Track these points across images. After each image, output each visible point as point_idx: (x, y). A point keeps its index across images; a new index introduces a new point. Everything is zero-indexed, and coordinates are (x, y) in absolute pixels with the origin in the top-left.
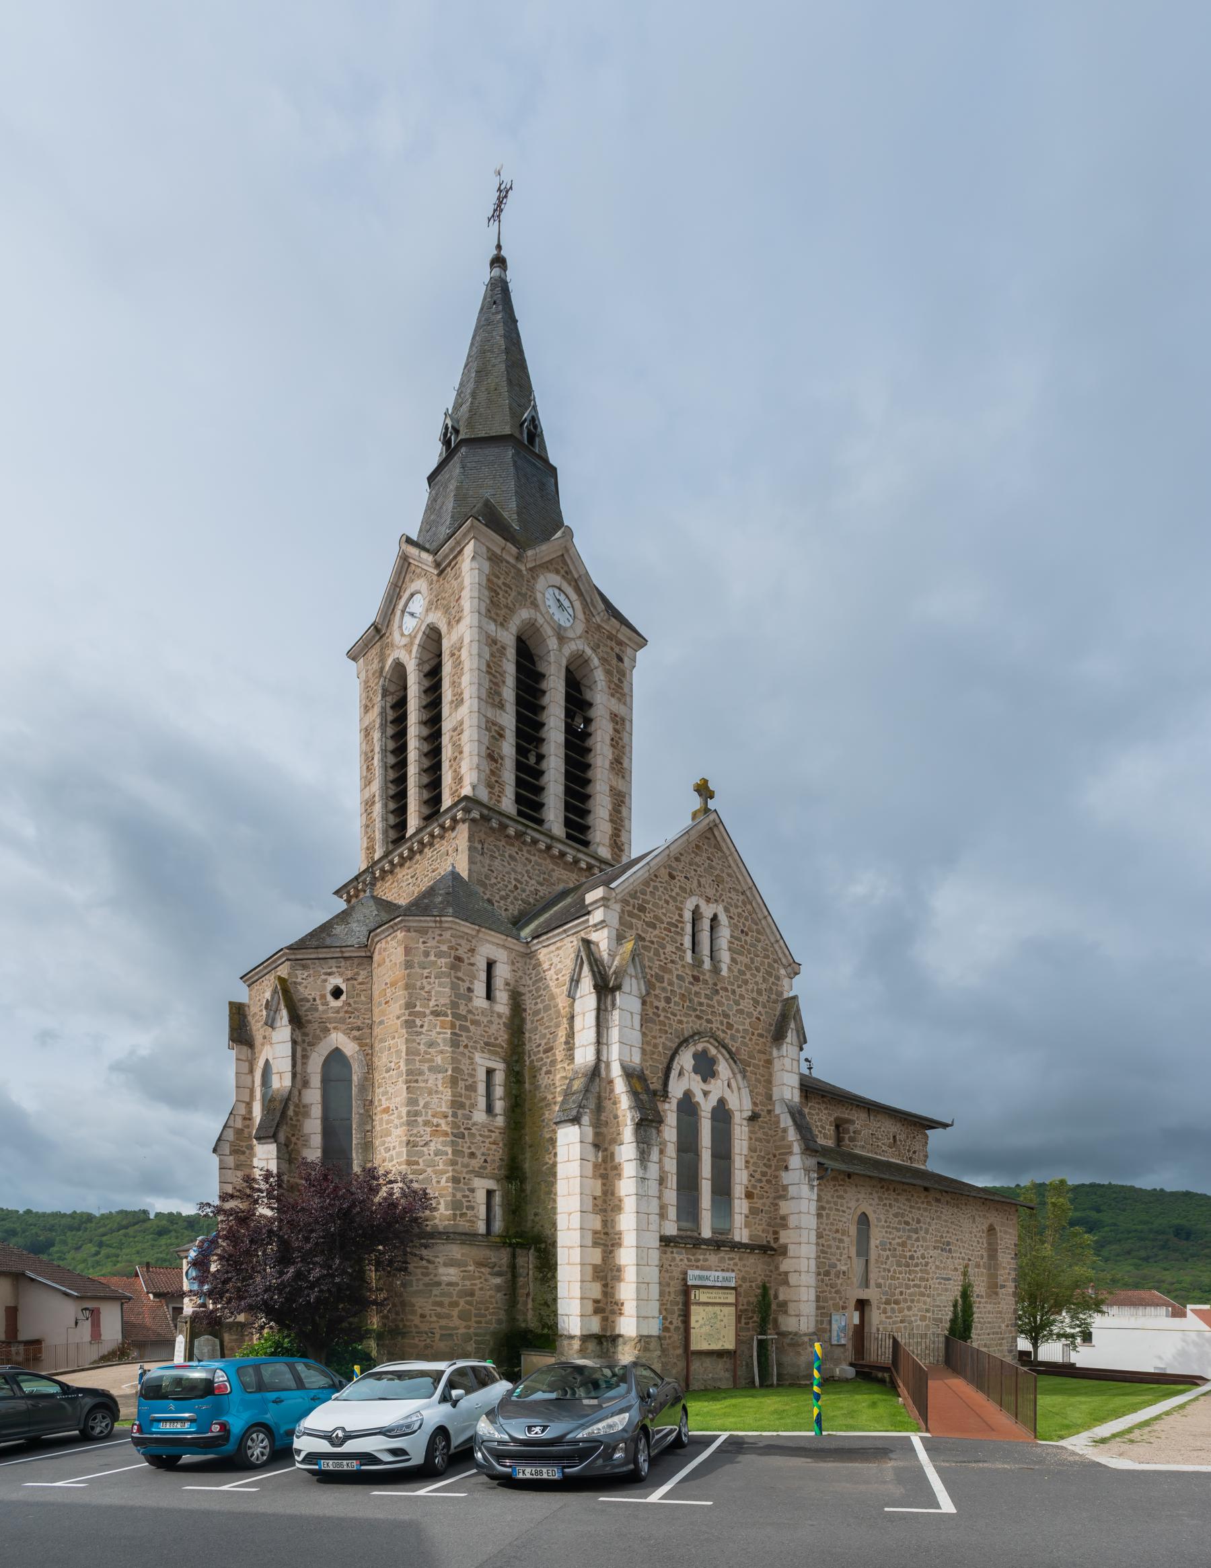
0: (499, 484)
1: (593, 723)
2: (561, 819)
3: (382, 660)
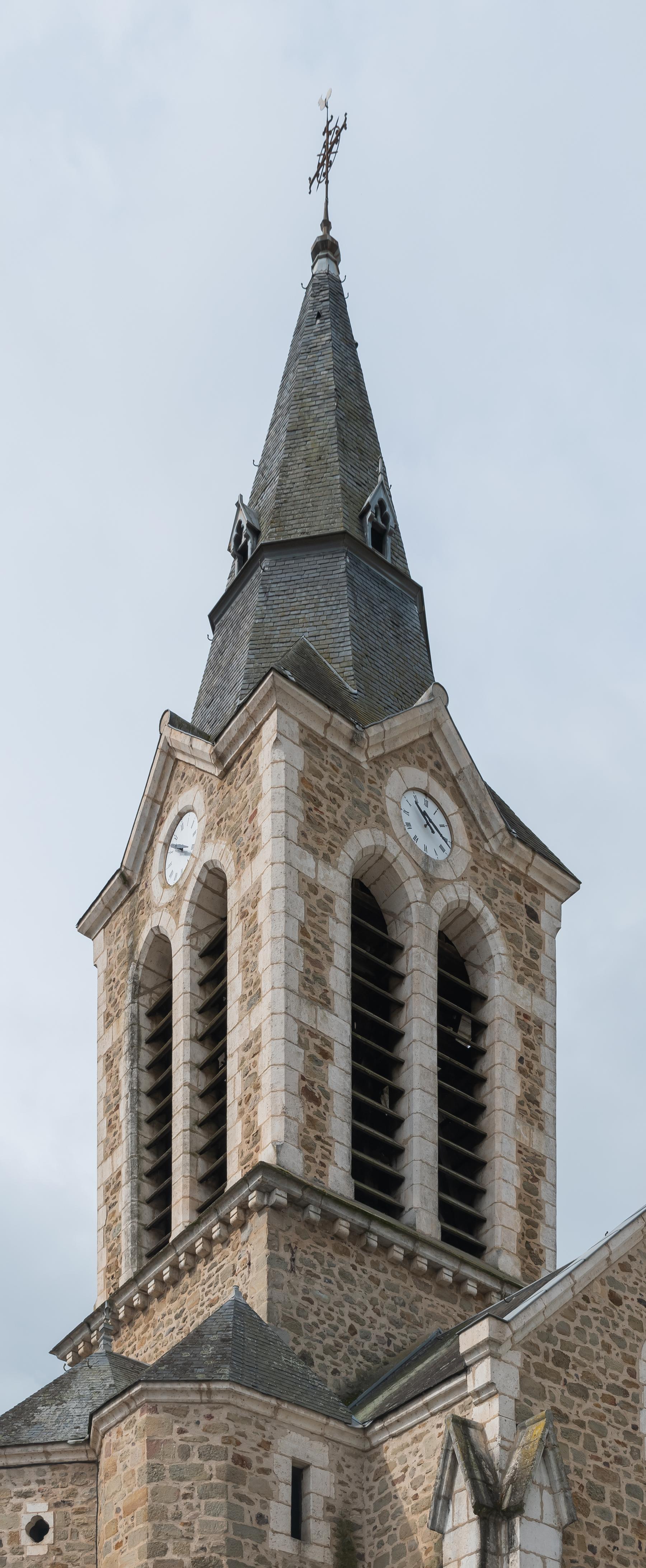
0: (323, 614)
1: (488, 1032)
2: (433, 1205)
3: (133, 933)
